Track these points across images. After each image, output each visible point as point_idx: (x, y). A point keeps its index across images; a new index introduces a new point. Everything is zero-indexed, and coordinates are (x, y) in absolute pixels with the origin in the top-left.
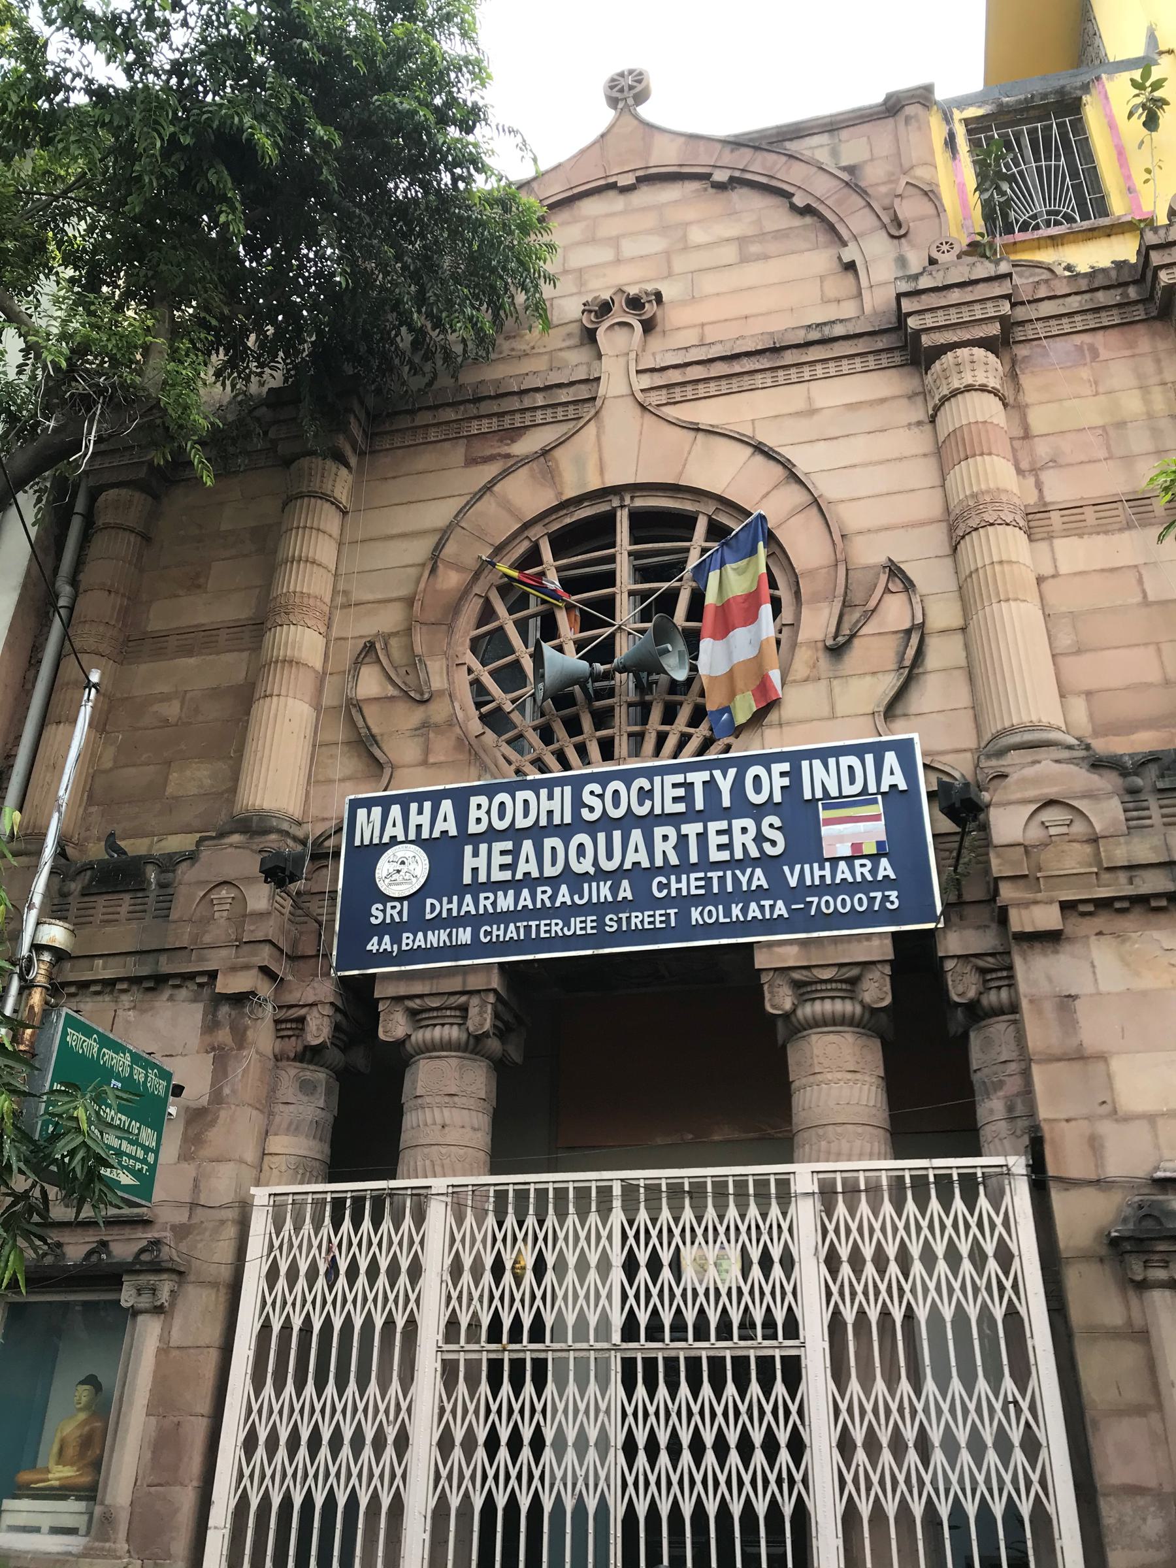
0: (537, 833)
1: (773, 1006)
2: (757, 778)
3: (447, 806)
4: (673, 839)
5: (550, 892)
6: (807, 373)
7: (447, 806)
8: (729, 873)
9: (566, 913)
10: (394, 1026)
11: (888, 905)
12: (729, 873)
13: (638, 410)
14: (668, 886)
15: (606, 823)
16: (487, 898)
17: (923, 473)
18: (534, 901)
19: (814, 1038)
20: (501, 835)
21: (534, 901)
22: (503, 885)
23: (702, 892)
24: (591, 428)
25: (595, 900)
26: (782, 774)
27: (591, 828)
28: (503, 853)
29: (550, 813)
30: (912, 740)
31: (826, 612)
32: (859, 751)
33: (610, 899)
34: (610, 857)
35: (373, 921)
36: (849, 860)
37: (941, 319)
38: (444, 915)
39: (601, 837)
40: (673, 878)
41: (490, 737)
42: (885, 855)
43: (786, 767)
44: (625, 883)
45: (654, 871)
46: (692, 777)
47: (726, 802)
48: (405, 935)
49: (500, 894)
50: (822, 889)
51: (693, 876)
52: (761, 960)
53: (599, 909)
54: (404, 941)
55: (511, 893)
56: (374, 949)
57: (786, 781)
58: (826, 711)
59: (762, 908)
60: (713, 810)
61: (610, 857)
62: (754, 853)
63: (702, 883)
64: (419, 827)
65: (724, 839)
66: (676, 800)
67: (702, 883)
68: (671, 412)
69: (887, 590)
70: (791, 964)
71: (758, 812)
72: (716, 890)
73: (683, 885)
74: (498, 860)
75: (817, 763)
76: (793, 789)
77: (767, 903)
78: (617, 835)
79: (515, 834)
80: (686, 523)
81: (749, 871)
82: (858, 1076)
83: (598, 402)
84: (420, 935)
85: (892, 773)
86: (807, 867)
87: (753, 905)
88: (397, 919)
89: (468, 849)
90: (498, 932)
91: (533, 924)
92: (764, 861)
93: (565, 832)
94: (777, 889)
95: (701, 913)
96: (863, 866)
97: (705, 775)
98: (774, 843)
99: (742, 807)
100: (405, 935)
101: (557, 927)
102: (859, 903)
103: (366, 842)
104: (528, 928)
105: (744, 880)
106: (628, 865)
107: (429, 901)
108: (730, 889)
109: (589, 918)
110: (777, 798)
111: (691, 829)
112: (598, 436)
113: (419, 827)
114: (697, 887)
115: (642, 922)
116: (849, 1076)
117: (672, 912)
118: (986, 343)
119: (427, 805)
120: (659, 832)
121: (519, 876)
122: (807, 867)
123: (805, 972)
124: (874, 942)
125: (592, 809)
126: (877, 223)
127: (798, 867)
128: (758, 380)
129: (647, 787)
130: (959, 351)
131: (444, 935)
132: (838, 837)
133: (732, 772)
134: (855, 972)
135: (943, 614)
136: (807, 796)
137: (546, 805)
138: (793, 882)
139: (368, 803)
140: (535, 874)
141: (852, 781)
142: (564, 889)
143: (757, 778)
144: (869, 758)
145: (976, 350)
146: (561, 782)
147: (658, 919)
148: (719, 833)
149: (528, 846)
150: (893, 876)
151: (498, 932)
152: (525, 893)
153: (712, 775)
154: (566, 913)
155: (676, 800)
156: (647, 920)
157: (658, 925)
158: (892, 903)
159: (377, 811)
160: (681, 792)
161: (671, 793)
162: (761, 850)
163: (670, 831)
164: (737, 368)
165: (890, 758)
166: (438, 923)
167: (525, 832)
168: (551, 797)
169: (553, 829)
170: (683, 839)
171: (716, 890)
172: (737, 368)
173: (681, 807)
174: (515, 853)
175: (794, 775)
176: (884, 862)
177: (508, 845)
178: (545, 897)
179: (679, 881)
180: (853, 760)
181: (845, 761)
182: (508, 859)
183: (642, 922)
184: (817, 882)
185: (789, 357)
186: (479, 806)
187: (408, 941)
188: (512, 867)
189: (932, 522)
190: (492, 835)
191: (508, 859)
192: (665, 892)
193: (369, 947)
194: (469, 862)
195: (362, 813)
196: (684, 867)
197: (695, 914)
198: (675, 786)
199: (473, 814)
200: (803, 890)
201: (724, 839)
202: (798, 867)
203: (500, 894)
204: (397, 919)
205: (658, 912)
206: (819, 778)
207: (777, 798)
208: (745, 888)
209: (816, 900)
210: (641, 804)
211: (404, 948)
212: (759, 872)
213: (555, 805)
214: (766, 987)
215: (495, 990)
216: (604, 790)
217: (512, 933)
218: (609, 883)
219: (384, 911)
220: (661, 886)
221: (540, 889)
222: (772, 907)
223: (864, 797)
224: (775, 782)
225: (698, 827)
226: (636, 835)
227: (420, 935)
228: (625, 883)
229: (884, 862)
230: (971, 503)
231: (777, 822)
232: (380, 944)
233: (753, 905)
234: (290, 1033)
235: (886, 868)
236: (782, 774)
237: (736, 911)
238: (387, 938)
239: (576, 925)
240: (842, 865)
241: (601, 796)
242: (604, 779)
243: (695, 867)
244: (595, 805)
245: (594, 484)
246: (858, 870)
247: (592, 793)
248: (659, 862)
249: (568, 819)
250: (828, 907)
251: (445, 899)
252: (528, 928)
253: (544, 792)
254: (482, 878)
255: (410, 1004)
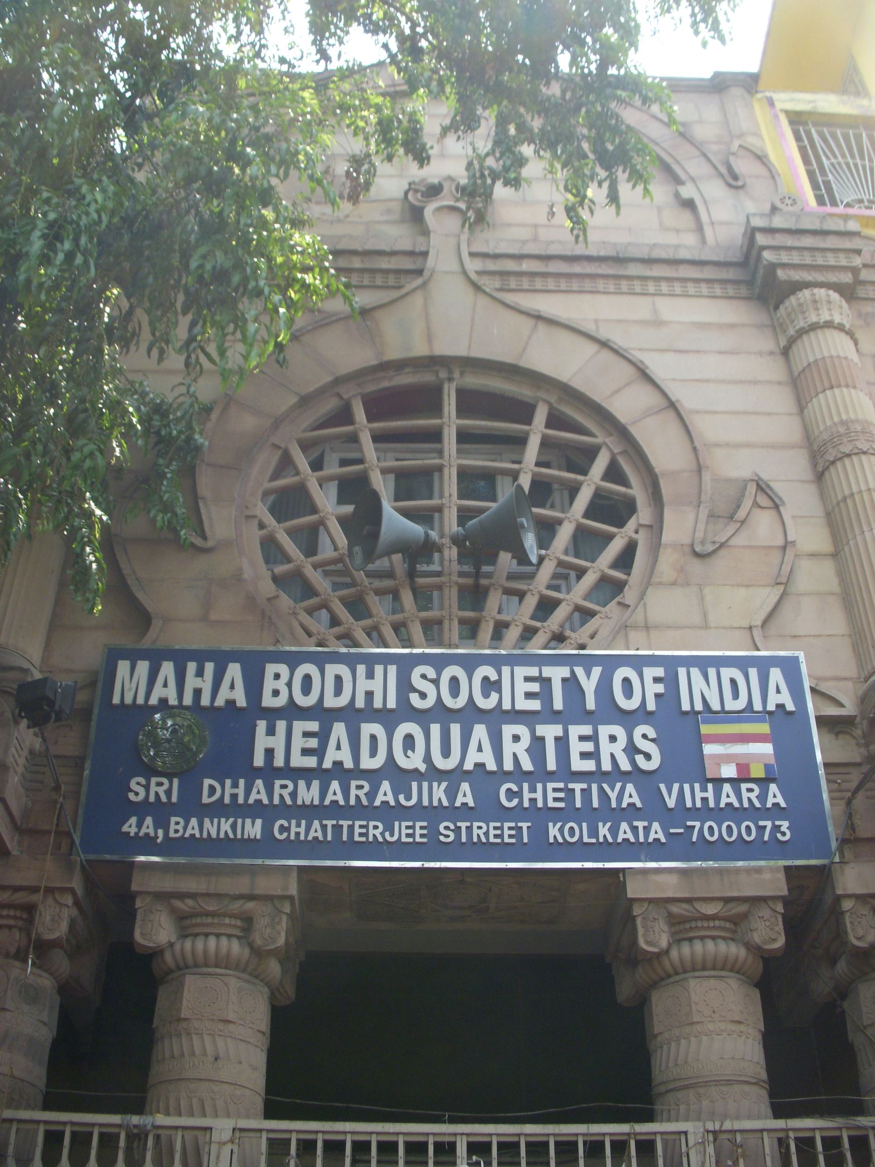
0: (352, 716)
1: (648, 943)
2: (626, 681)
3: (234, 670)
4: (526, 741)
5: (367, 788)
6: (651, 287)
7: (234, 670)
8: (594, 787)
9: (389, 814)
10: (155, 930)
11: (779, 835)
12: (594, 787)
13: (470, 291)
14: (519, 794)
15: (441, 713)
16: (284, 787)
17: (781, 400)
18: (346, 796)
19: (692, 983)
20: (305, 713)
21: (346, 796)
22: (306, 774)
23: (561, 805)
24: (418, 299)
25: (426, 803)
26: (657, 680)
27: (423, 717)
28: (306, 734)
29: (369, 695)
30: (796, 659)
31: (691, 517)
32: (743, 664)
33: (445, 803)
34: (446, 752)
35: (132, 796)
36: (735, 782)
37: (795, 258)
38: (227, 800)
39: (435, 729)
40: (526, 786)
41: (285, 602)
42: (773, 780)
43: (660, 672)
44: (465, 786)
45: (502, 775)
46: (547, 672)
47: (591, 705)
48: (174, 819)
49: (302, 784)
50: (705, 812)
51: (550, 786)
52: (633, 890)
53: (432, 814)
54: (173, 827)
55: (316, 784)
56: (133, 831)
57: (660, 688)
58: (697, 619)
59: (635, 829)
60: (575, 711)
61: (446, 752)
62: (625, 765)
63: (562, 795)
64: (198, 692)
65: (589, 747)
66: (529, 695)
67: (562, 795)
68: (509, 298)
69: (756, 505)
70: (670, 894)
71: (629, 719)
72: (578, 804)
73: (539, 795)
74: (298, 742)
75: (695, 672)
76: (669, 696)
77: (641, 824)
78: (455, 730)
79: (325, 716)
80: (523, 412)
81: (619, 785)
82: (742, 1028)
83: (426, 274)
84: (194, 822)
85: (778, 691)
86: (686, 787)
87: (624, 826)
88: (164, 798)
89: (262, 726)
90: (297, 829)
91: (345, 823)
92: (637, 775)
93: (389, 719)
94: (654, 807)
95: (561, 830)
96: (750, 790)
97: (565, 672)
98: (648, 757)
99: (608, 710)
100: (174, 819)
101: (376, 830)
102: (746, 829)
103: (128, 700)
104: (338, 828)
105: (613, 796)
106: (469, 766)
107: (207, 782)
108: (595, 804)
109: (419, 824)
110: (651, 706)
111: (550, 732)
112: (426, 306)
113: (198, 692)
114: (556, 800)
115: (486, 834)
116: (733, 1027)
117: (525, 825)
118: (838, 288)
119: (209, 667)
120: (508, 730)
121: (327, 764)
122: (686, 787)
123: (685, 906)
124: (766, 877)
125: (423, 696)
126: (713, 172)
127: (676, 786)
128: (600, 285)
129: (494, 677)
130: (816, 290)
131: (226, 826)
132: (721, 755)
133: (597, 671)
134: (743, 908)
135: (811, 536)
136: (686, 706)
137: (363, 685)
138: (671, 803)
139: (133, 657)
140: (349, 764)
141: (736, 695)
142: (386, 786)
143: (626, 681)
144: (753, 672)
145: (831, 292)
146: (386, 660)
147: (507, 832)
148: (582, 738)
149: (339, 730)
150: (783, 804)
151: (297, 829)
152: (335, 785)
153: (573, 673)
154: (389, 814)
155: (529, 695)
156: (492, 832)
157: (507, 840)
158: (784, 834)
159: (143, 667)
160: (535, 687)
161: (522, 687)
162: (633, 762)
163: (522, 730)
164: (577, 269)
165: (776, 675)
166: (218, 810)
167: (336, 714)
168: (370, 675)
169: (371, 714)
170: (538, 742)
171: (578, 804)
172: (577, 269)
173: (535, 705)
174: (323, 736)
175: (671, 681)
176: (773, 788)
177: (313, 726)
178: (361, 793)
179: (533, 790)
180: (735, 673)
181: (728, 673)
182: (313, 743)
183: (486, 834)
184: (699, 804)
185: (633, 270)
186: (277, 676)
187: (176, 826)
188: (319, 753)
189: (792, 447)
190: (292, 712)
191: (313, 743)
192: (515, 802)
193: (125, 828)
194: (262, 741)
195: (123, 667)
196: (541, 774)
197: (553, 831)
198: (527, 679)
199: (269, 684)
200: (683, 812)
201: (589, 747)
202: (676, 786)
203: (302, 784)
204: (164, 798)
205: (507, 825)
206: (696, 690)
207: (651, 706)
208: (614, 805)
209: (697, 824)
210: (486, 695)
211: (172, 834)
212: (630, 788)
213: (376, 685)
214: (639, 921)
215: (291, 898)
216: (439, 674)
217: (316, 831)
218: (444, 785)
219: (147, 788)
220: (510, 794)
221: (354, 784)
222: (647, 829)
223: (748, 713)
224: (648, 689)
225: (556, 730)
226: (480, 732)
227: (194, 822)
228: (465, 786)
229: (773, 788)
230: (842, 430)
231: (652, 733)
232: (140, 825)
233: (624, 826)
234: (12, 922)
235: (775, 795)
236: (657, 680)
237: (604, 830)
238: (149, 820)
239: (401, 831)
240: (727, 788)
241: (436, 682)
242: (439, 663)
243: (551, 776)
244: (427, 691)
245: (420, 350)
246: (745, 795)
247: (424, 676)
248: (508, 766)
249: (392, 704)
250: (712, 833)
251: (228, 782)
252: (338, 828)
253: (361, 669)
254: (279, 762)
255: (178, 904)
